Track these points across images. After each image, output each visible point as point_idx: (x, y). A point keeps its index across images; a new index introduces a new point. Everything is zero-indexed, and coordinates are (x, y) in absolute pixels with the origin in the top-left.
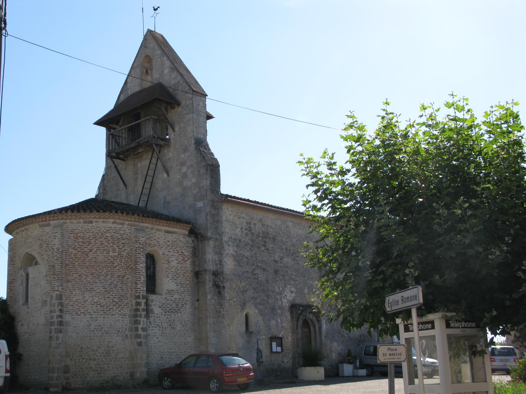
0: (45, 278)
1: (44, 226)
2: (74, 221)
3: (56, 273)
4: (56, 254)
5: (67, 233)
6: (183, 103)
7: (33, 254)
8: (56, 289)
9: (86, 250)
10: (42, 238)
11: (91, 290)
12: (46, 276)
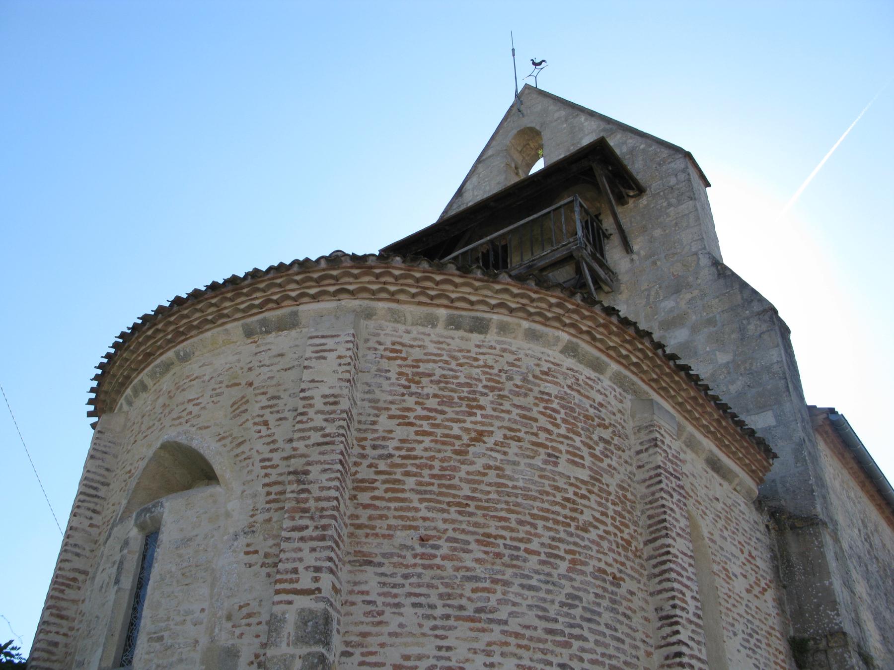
0: (243, 541)
1: (268, 328)
2: (411, 311)
3: (311, 504)
4: (319, 420)
5: (371, 355)
6: (654, 186)
7: (195, 444)
8: (305, 581)
9: (456, 430)
10: (251, 377)
11: (479, 618)
12: (250, 530)
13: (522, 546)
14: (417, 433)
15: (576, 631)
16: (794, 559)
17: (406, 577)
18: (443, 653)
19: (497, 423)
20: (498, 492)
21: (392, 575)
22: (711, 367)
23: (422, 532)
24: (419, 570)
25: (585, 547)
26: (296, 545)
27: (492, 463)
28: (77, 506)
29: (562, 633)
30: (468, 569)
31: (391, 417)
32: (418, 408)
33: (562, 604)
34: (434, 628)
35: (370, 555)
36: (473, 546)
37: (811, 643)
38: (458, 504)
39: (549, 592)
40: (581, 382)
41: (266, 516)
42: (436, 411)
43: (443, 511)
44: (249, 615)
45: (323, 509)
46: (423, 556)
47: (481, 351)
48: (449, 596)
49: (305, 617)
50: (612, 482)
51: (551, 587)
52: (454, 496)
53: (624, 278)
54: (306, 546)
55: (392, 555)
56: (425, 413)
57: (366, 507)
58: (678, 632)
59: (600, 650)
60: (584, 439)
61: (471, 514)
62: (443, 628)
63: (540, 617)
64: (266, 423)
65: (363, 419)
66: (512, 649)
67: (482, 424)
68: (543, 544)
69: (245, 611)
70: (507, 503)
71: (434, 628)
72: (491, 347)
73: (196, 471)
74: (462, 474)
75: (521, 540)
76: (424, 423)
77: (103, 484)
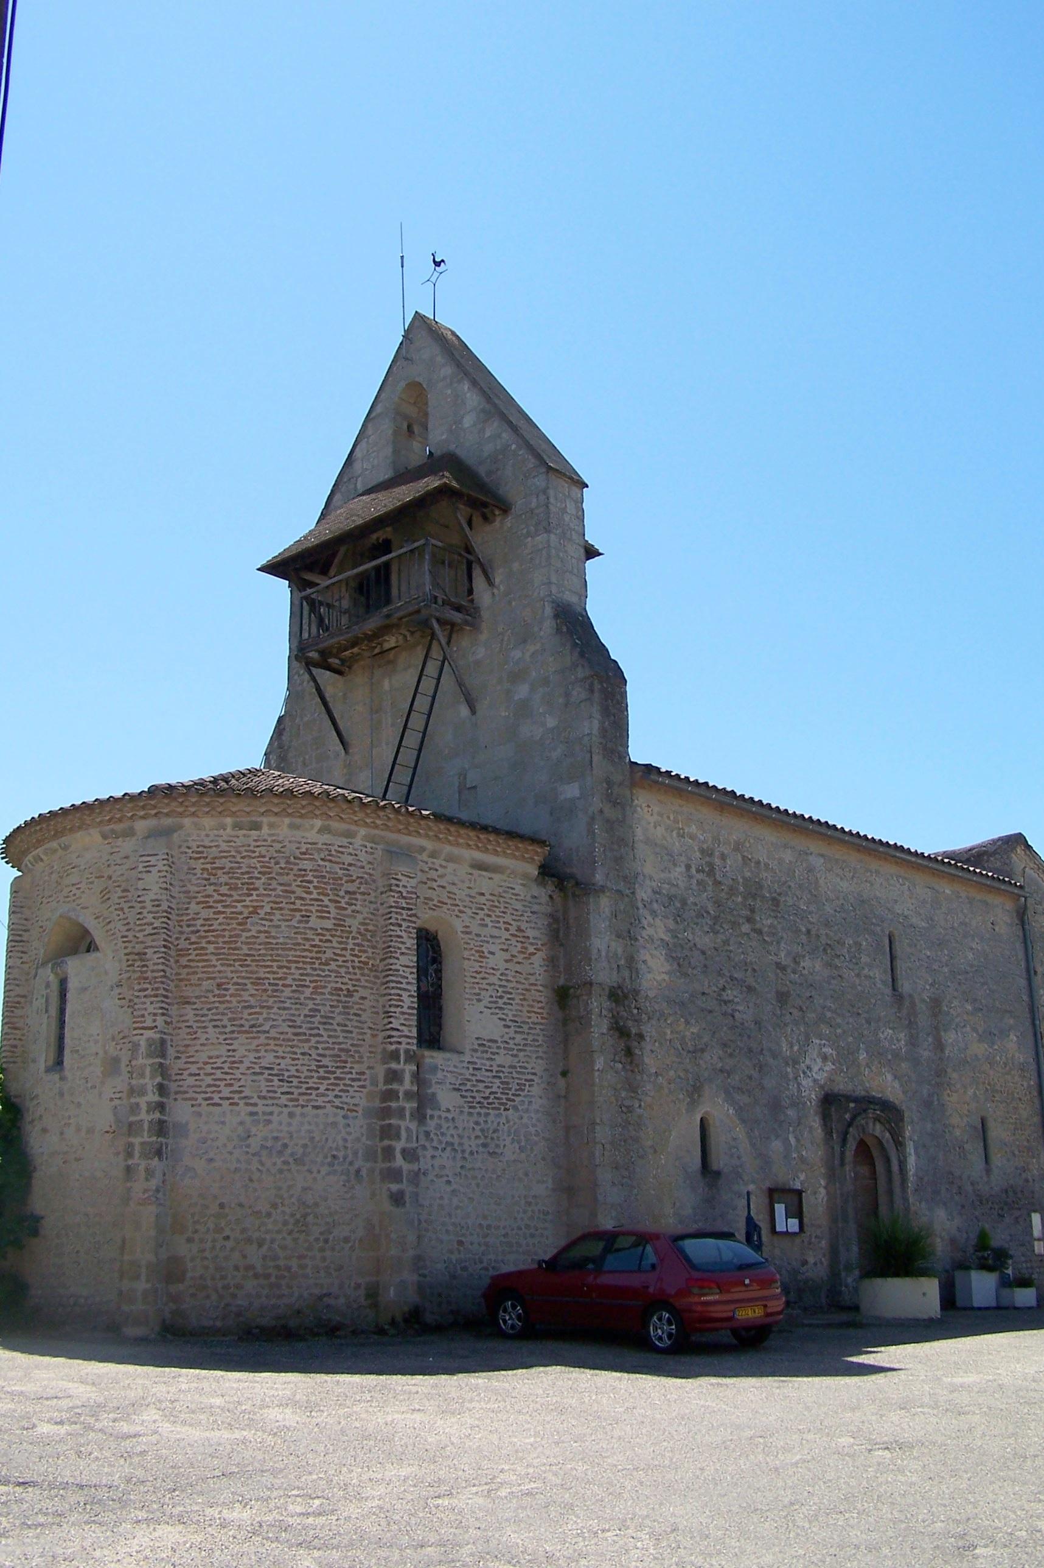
0: (117, 990)
3: (149, 974)
6: (519, 504)
8: (149, 1023)
13: (281, 982)
14: (214, 913)
15: (315, 1031)
16: (571, 921)
17: (209, 1009)
18: (230, 1053)
19: (267, 899)
20: (266, 949)
21: (202, 1009)
22: (541, 730)
23: (219, 981)
24: (217, 1005)
25: (326, 976)
26: (143, 1000)
27: (262, 929)
28: (9, 951)
29: (305, 1034)
30: (246, 1001)
31: (198, 903)
32: (215, 894)
33: (306, 1016)
34: (225, 1039)
35: (188, 997)
36: (249, 986)
37: (572, 990)
38: (241, 960)
39: (296, 1009)
40: (333, 853)
41: (128, 975)
42: (226, 895)
43: (230, 965)
44: (124, 1038)
45: (156, 978)
46: (219, 996)
47: (259, 844)
48: (234, 1019)
49: (150, 1042)
50: (354, 924)
51: (298, 1006)
52: (238, 955)
53: (485, 614)
54: (148, 1001)
55: (201, 997)
56: (220, 898)
57: (186, 966)
58: (391, 1023)
59: (331, 1041)
60: (331, 897)
61: (248, 966)
62: (231, 1039)
63: (290, 1026)
64: (122, 909)
65: (180, 906)
66: (272, 1047)
67: (257, 901)
68: (294, 980)
69: (121, 1035)
70: (271, 955)
71: (225, 1039)
72: (265, 840)
73: (81, 942)
74: (243, 939)
75: (280, 979)
76: (219, 905)
77: (25, 931)
